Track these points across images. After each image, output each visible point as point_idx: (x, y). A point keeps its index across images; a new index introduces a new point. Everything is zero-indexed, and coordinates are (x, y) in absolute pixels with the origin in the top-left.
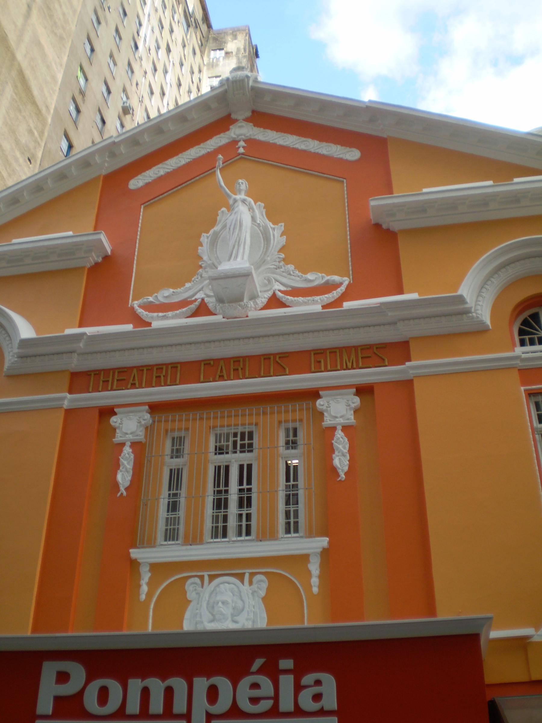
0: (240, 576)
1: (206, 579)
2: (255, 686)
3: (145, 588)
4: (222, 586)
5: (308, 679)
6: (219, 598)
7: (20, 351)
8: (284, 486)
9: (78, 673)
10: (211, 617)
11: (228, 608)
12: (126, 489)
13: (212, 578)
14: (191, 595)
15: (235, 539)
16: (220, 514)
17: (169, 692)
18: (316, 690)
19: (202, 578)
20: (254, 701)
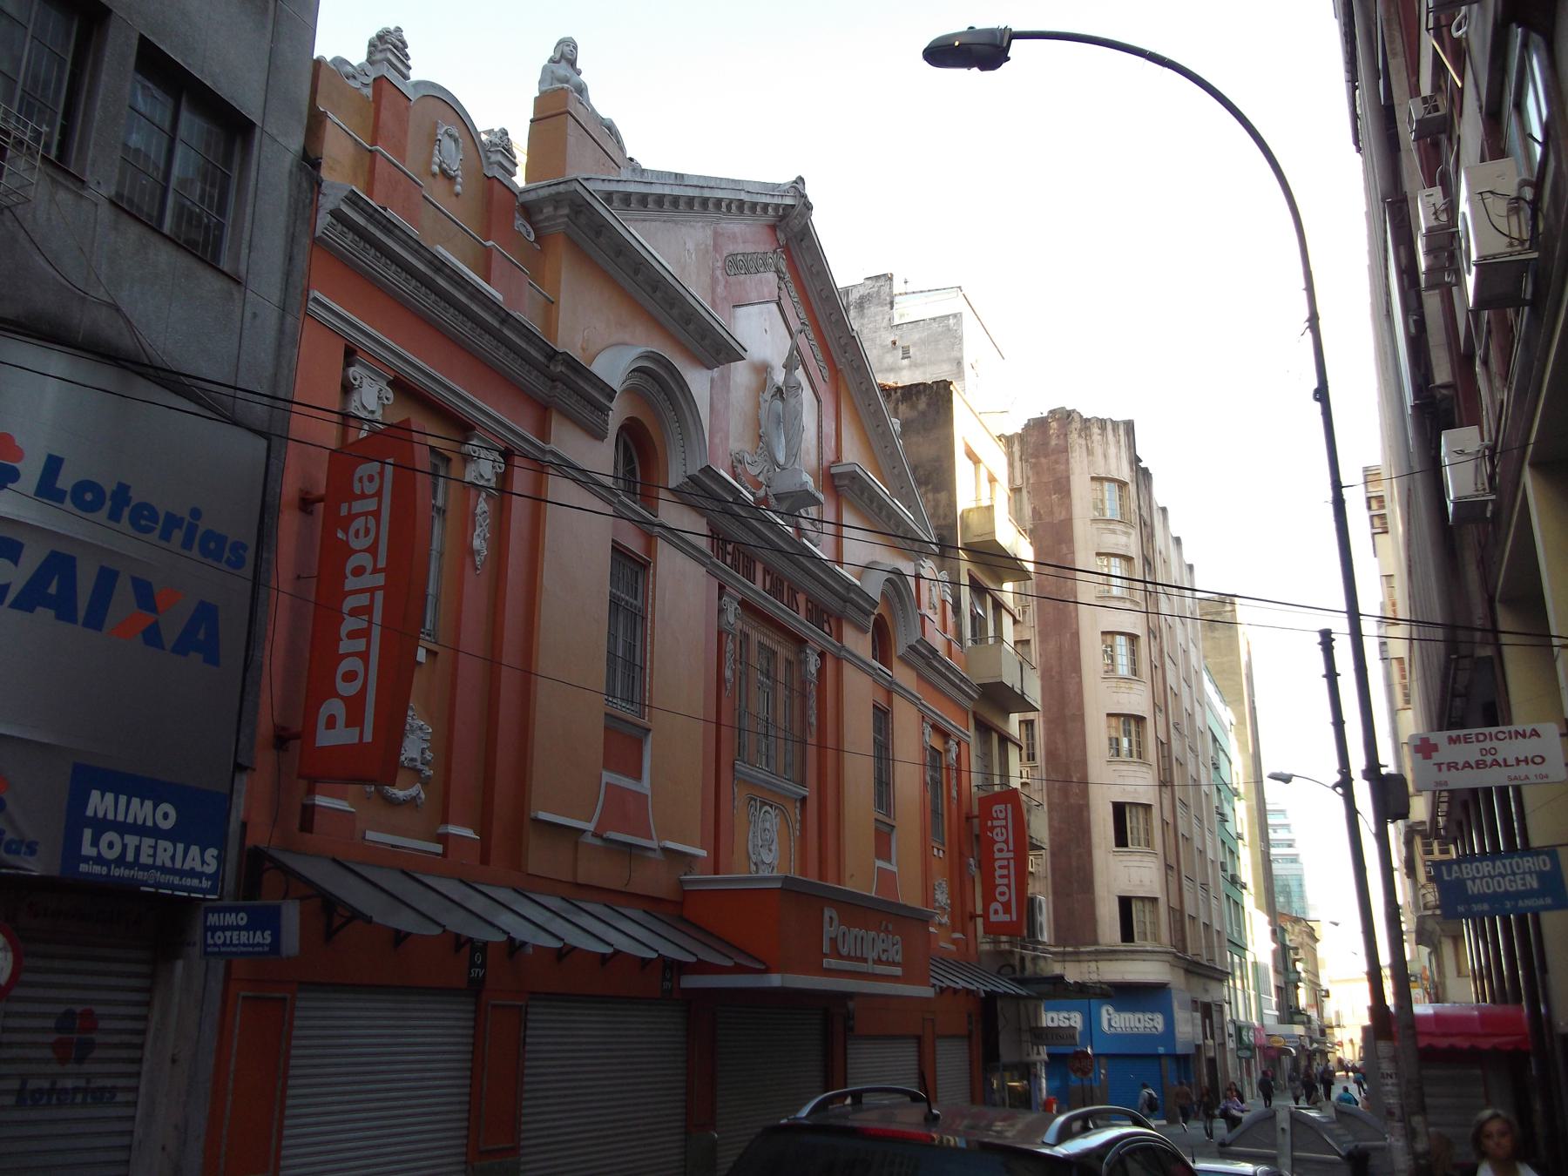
7: (1499, 1009)
9: (994, 906)
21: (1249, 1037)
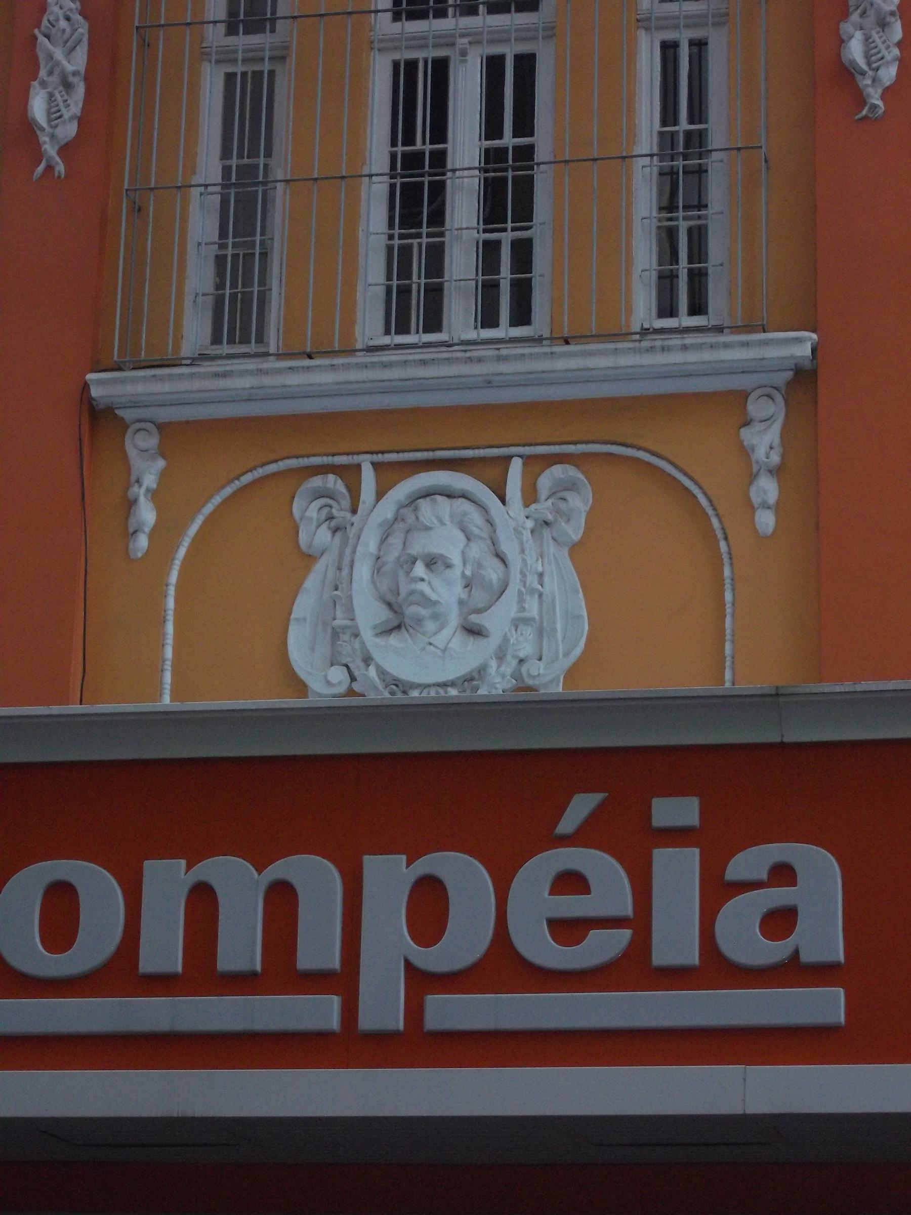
0: (492, 471)
1: (368, 477)
2: (571, 882)
3: (147, 514)
4: (424, 504)
5: (748, 863)
6: (420, 545)
8: (655, 139)
10: (384, 614)
11: (463, 600)
12: (65, 150)
13: (389, 474)
14: (315, 535)
15: (472, 335)
16: (415, 242)
17: (282, 900)
18: (778, 896)
19: (350, 474)
20: (568, 930)
21: (268, 292)
